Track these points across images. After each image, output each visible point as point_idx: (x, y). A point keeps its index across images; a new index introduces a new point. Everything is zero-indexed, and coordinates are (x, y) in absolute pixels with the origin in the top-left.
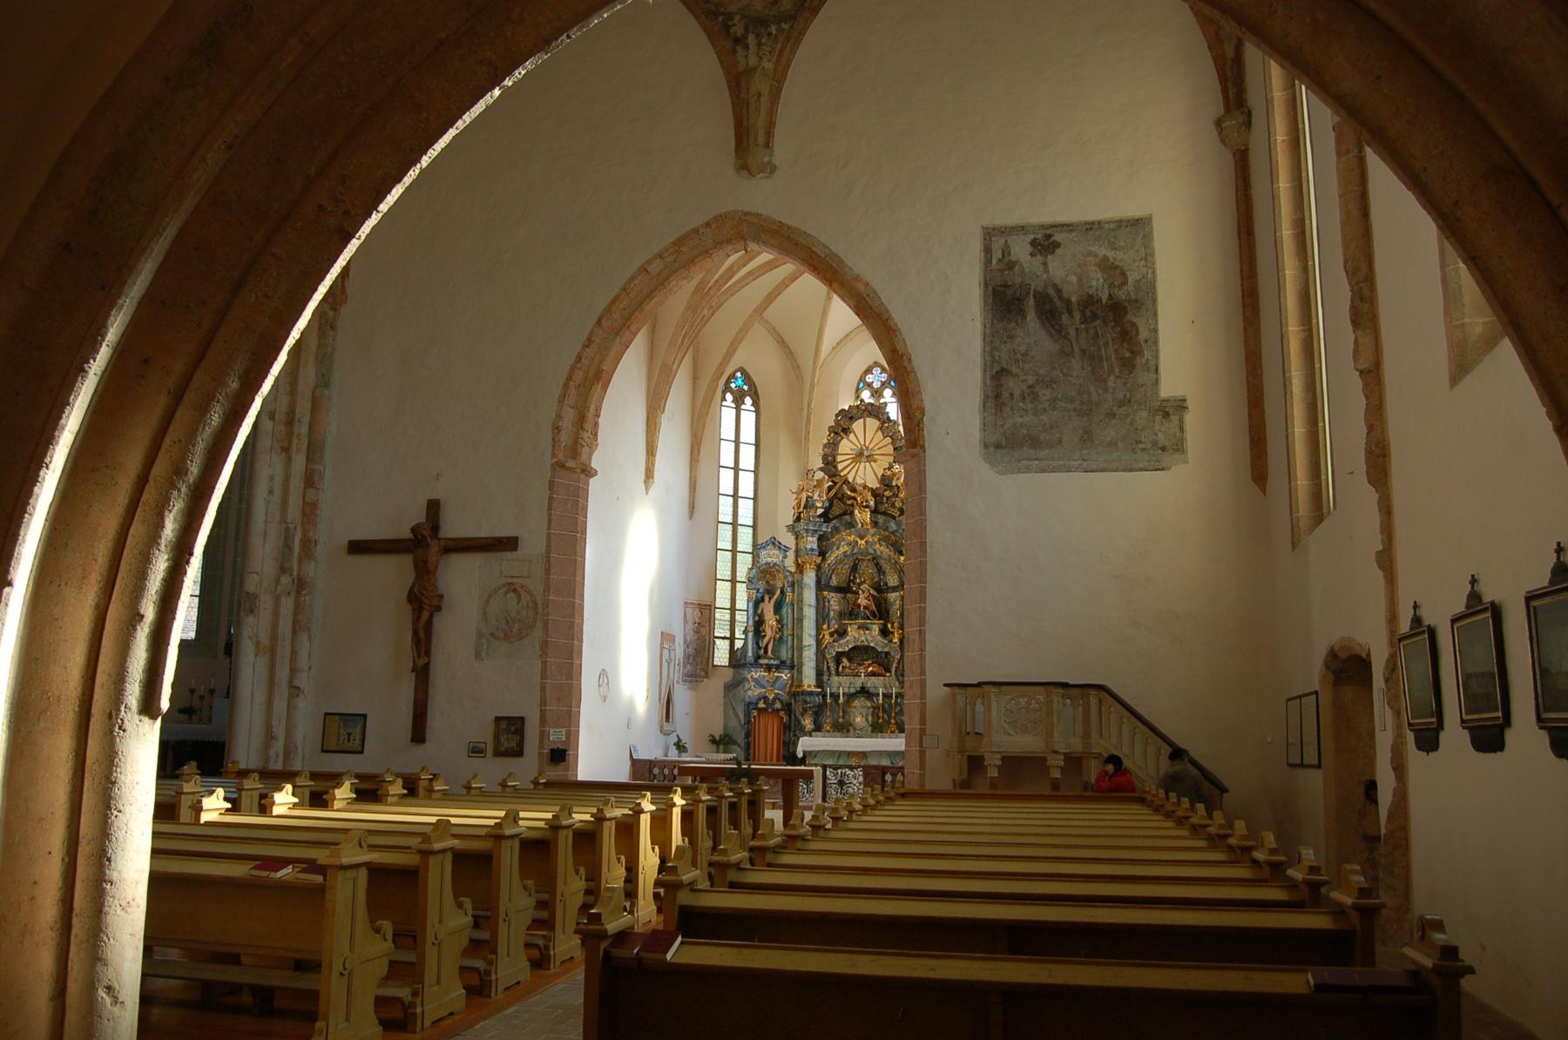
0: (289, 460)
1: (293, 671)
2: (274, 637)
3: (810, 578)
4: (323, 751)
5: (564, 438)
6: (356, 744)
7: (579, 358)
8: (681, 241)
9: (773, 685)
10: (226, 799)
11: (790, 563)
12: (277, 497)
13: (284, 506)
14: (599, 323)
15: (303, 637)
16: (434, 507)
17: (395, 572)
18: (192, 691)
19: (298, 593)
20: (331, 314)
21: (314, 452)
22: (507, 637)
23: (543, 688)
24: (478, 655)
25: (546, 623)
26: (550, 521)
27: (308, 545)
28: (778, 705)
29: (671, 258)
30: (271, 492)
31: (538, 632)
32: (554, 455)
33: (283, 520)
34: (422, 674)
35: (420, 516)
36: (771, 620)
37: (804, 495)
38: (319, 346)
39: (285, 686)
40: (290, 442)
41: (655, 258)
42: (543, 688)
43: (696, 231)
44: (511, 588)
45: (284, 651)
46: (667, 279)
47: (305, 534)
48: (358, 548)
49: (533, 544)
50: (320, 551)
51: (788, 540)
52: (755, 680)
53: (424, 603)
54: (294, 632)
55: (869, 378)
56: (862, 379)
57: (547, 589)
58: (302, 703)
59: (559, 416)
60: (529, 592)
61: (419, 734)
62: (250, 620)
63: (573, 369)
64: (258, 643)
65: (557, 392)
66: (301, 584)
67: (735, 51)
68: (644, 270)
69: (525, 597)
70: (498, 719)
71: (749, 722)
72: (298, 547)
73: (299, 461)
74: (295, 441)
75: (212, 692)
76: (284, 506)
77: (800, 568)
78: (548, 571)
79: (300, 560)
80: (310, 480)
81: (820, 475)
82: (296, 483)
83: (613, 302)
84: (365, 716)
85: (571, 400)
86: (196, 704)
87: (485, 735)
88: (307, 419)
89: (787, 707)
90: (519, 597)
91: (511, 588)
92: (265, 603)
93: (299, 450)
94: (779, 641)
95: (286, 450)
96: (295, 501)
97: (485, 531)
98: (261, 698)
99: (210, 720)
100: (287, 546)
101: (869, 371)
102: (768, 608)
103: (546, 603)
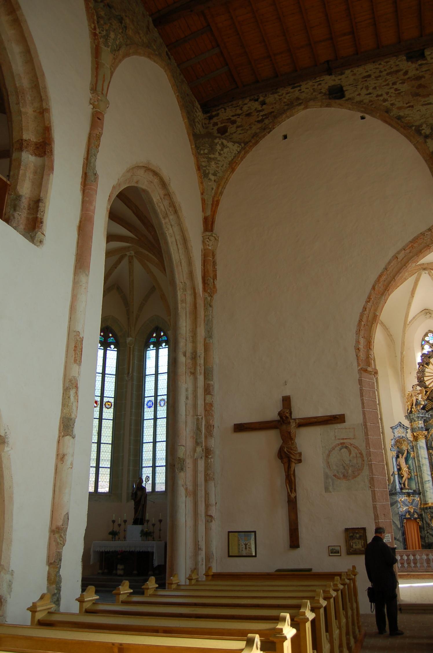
0: (195, 379)
1: (207, 506)
2: (195, 484)
3: (422, 443)
4: (229, 556)
5: (362, 355)
6: (331, 554)
7: (365, 309)
8: (415, 240)
9: (412, 504)
10: (130, 587)
11: (409, 436)
12: (190, 402)
13: (195, 406)
14: (373, 288)
15: (212, 484)
16: (287, 401)
17: (267, 442)
18: (114, 522)
19: (207, 457)
20: (209, 298)
21: (208, 374)
22: (345, 477)
23: (375, 508)
24: (327, 489)
25: (370, 466)
26: (363, 403)
27: (209, 428)
28: (416, 516)
29: (408, 251)
30: (187, 398)
31: (366, 472)
32: (359, 365)
33: (195, 414)
34: (292, 504)
35: (279, 407)
36: (405, 468)
37: (414, 399)
38: (205, 316)
39: (203, 515)
40: (195, 369)
41: (401, 250)
42: (375, 508)
43: (423, 234)
44: (343, 446)
45: (201, 493)
46: (408, 262)
47: (207, 422)
48: (240, 428)
49: (354, 418)
50: (215, 431)
51: (406, 423)
52: (403, 502)
53: (288, 457)
54: (206, 481)
55: (427, 339)
56: (423, 340)
57: (368, 444)
58: (215, 525)
59: (358, 342)
60: (356, 447)
61: (294, 542)
62: (182, 474)
63: (362, 315)
64: (186, 489)
65: (354, 329)
66: (208, 452)
67: (426, 142)
68: (395, 257)
69: (354, 452)
70: (347, 530)
71: (403, 526)
72: (204, 429)
73: (201, 379)
74: (198, 368)
75: (125, 521)
76: (195, 406)
77: (416, 438)
78: (366, 434)
79: (206, 437)
80: (208, 390)
81: (419, 388)
82: (200, 392)
83: (380, 276)
84: (255, 532)
85: (362, 333)
86: (116, 529)
87: (340, 542)
88: (202, 356)
89: (421, 516)
90: (350, 452)
91: (343, 446)
92: (189, 463)
93: (201, 373)
94: (410, 479)
95: (193, 373)
96: (200, 402)
97: (321, 412)
98: (190, 522)
99: (125, 538)
100: (198, 429)
101: (426, 335)
102: (402, 461)
103: (369, 454)
